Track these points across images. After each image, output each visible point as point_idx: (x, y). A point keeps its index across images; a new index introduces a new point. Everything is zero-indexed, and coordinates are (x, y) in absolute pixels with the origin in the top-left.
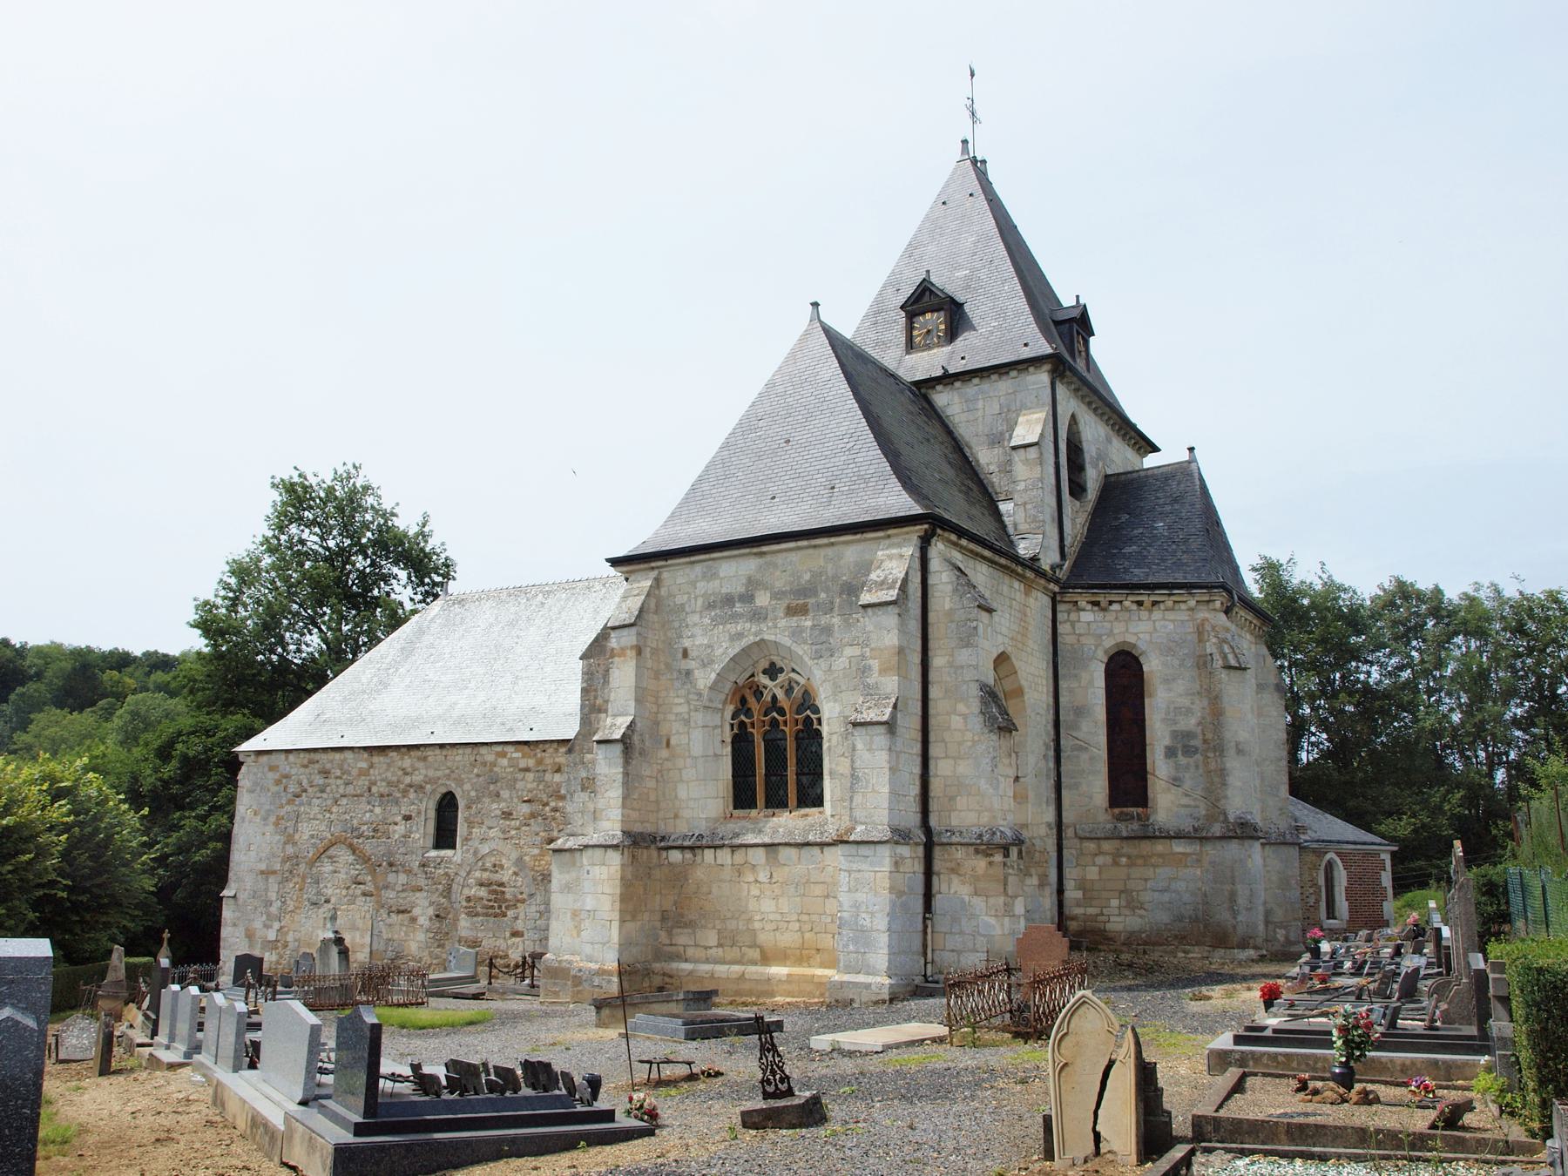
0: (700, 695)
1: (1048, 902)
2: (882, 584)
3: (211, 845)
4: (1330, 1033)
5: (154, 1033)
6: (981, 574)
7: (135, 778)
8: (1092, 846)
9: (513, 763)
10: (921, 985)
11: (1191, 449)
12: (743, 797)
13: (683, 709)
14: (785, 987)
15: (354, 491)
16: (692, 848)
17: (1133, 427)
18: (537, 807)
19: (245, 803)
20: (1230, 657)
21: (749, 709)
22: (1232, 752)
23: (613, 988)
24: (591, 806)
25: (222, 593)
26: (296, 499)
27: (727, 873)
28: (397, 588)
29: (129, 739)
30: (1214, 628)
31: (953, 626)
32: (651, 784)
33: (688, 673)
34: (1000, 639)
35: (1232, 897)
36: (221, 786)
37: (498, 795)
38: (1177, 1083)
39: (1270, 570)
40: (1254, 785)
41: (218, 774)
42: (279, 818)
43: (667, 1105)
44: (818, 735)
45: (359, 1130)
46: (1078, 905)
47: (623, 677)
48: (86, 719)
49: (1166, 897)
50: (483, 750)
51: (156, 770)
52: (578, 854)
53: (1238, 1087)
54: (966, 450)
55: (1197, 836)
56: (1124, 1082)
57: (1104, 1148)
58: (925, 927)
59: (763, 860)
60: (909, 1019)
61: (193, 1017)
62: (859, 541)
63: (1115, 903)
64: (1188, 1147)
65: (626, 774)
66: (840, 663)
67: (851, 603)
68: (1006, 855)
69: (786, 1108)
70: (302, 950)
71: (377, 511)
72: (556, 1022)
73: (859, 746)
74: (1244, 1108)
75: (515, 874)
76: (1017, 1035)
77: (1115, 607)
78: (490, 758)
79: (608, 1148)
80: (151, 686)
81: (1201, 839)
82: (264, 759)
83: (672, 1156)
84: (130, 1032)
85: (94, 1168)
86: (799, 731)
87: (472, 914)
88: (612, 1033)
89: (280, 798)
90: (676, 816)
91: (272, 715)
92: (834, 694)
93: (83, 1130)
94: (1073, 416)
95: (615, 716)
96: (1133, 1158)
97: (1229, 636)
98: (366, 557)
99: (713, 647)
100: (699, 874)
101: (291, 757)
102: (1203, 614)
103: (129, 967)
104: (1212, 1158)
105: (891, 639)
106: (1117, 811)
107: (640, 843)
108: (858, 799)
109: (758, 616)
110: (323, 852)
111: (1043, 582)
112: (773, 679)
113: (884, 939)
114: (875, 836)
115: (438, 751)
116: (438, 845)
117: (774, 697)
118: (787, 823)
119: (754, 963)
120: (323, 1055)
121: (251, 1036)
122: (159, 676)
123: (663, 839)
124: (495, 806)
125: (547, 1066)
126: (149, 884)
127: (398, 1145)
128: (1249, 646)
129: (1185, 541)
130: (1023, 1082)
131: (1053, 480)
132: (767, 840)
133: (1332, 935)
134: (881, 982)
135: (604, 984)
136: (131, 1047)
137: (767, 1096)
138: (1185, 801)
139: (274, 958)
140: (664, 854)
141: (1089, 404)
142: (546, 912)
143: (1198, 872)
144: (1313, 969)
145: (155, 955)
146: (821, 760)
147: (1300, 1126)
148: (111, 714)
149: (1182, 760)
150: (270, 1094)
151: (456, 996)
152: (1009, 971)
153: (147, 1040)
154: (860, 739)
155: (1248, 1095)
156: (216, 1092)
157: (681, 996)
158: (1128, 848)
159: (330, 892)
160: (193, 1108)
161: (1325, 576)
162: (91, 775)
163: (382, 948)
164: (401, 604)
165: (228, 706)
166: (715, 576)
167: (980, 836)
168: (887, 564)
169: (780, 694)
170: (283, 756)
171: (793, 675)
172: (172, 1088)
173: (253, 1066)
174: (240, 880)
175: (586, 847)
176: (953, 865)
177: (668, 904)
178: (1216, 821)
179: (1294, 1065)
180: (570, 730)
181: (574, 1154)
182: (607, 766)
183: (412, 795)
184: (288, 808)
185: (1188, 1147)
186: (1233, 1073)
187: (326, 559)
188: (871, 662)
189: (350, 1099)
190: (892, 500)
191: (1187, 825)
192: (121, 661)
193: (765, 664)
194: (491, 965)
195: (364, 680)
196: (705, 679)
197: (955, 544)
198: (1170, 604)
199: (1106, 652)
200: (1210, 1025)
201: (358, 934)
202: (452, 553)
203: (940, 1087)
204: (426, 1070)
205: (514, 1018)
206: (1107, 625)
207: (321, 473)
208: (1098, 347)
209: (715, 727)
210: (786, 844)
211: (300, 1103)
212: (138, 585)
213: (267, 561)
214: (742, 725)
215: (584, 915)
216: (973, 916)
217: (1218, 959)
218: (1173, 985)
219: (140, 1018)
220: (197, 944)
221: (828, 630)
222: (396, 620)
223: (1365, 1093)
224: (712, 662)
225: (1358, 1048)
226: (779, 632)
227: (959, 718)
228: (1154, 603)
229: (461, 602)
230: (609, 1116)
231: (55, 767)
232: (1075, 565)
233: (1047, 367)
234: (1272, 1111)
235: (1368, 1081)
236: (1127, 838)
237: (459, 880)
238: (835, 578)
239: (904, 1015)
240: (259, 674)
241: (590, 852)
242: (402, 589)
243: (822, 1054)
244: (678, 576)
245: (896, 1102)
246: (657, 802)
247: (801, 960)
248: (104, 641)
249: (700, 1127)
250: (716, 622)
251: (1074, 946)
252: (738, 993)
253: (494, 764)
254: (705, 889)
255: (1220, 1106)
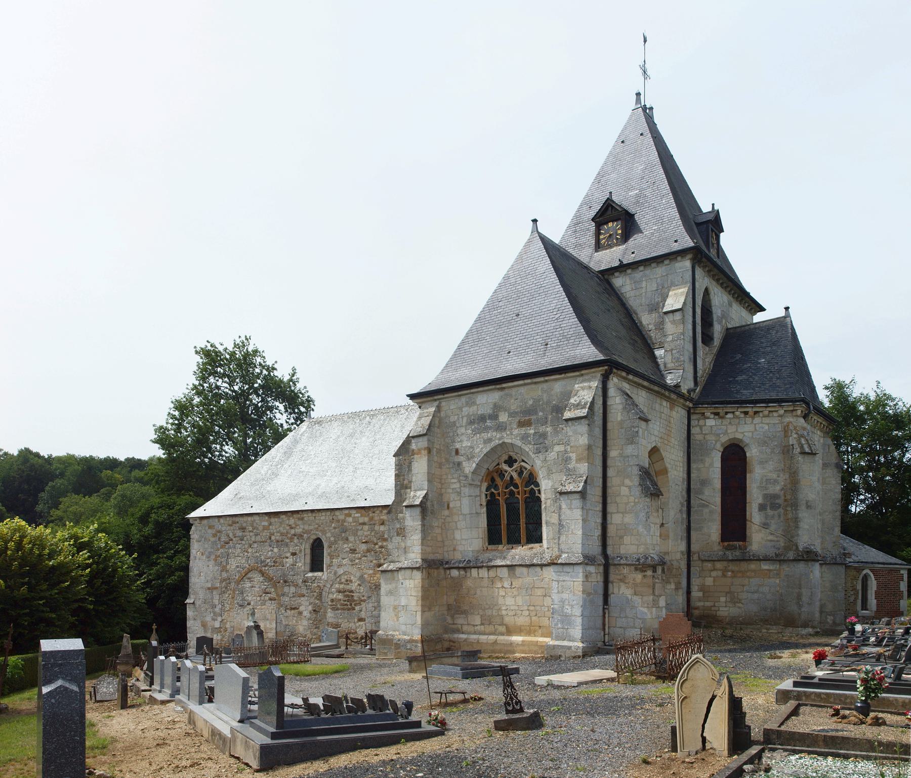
0: (466, 477)
1: (681, 599)
2: (578, 406)
3: (177, 574)
4: (855, 682)
5: (152, 684)
6: (641, 397)
7: (127, 535)
8: (709, 565)
9: (355, 520)
10: (599, 647)
11: (787, 309)
12: (493, 538)
13: (457, 486)
14: (521, 648)
15: (247, 355)
16: (464, 568)
17: (747, 295)
18: (371, 546)
19: (195, 549)
20: (806, 447)
21: (496, 485)
22: (803, 507)
23: (418, 650)
24: (403, 545)
25: (171, 421)
26: (211, 360)
27: (486, 582)
28: (278, 415)
29: (122, 511)
30: (795, 428)
31: (623, 431)
32: (438, 531)
33: (459, 464)
34: (653, 438)
35: (799, 597)
36: (180, 538)
37: (347, 539)
38: (756, 709)
39: (839, 390)
40: (816, 528)
41: (177, 531)
42: (217, 557)
43: (451, 718)
44: (539, 500)
45: (274, 736)
46: (700, 601)
47: (420, 467)
48: (93, 500)
49: (756, 596)
50: (337, 513)
51: (140, 530)
52: (396, 573)
53: (795, 712)
54: (634, 315)
55: (778, 559)
56: (721, 709)
57: (708, 746)
58: (604, 613)
59: (506, 575)
60: (594, 667)
61: (173, 675)
62: (563, 378)
63: (723, 599)
64: (759, 747)
65: (423, 525)
66: (552, 455)
67: (558, 418)
68: (655, 571)
69: (519, 719)
70: (236, 633)
71: (263, 367)
72: (386, 670)
73: (564, 506)
74: (796, 725)
75: (359, 585)
76: (658, 678)
77: (730, 416)
78: (341, 517)
79: (418, 743)
80: (132, 479)
81: (780, 561)
82: (205, 522)
83: (455, 746)
84: (138, 684)
85: (122, 761)
86: (527, 498)
87: (334, 609)
88: (418, 676)
89: (217, 545)
90: (454, 550)
91: (209, 495)
92: (548, 475)
93: (114, 740)
94: (706, 290)
95: (416, 490)
96: (726, 752)
97: (805, 433)
98: (258, 395)
99: (474, 447)
100: (469, 583)
101: (222, 520)
102: (788, 419)
103: (133, 645)
104: (775, 754)
105: (583, 440)
106: (726, 544)
107: (434, 567)
108: (563, 538)
109: (501, 428)
110: (245, 575)
111: (682, 401)
112: (511, 466)
113: (579, 621)
114: (573, 560)
115: (310, 514)
116: (313, 570)
117: (512, 477)
118: (521, 553)
119: (502, 634)
120: (251, 693)
121: (208, 684)
122: (137, 473)
123: (447, 563)
124: (346, 546)
125: (381, 697)
126: (141, 598)
127: (297, 744)
128: (819, 439)
129: (779, 371)
130: (661, 705)
131: (691, 333)
132: (509, 563)
133: (863, 620)
134: (578, 645)
135: (413, 648)
136: (138, 692)
137: (508, 712)
138: (771, 537)
139: (219, 638)
140: (448, 572)
141: (717, 281)
142: (378, 607)
143: (778, 581)
144: (849, 641)
145: (148, 638)
146: (541, 514)
147: (832, 737)
148: (110, 497)
149: (770, 512)
150: (221, 717)
151: (327, 656)
152: (654, 640)
153: (148, 688)
154: (564, 503)
155: (801, 718)
156: (190, 717)
157: (460, 654)
158: (732, 567)
159: (250, 599)
160: (177, 726)
161: (878, 391)
162: (100, 535)
163: (283, 629)
164: (282, 425)
165: (180, 491)
166: (474, 403)
167: (638, 560)
168: (581, 393)
169: (515, 475)
170: (216, 520)
171: (523, 464)
172: (164, 715)
173: (210, 701)
174: (196, 593)
175: (401, 569)
176: (622, 577)
177: (451, 601)
178: (791, 550)
179: (832, 700)
180: (389, 499)
181: (399, 746)
182: (412, 521)
183: (296, 541)
184: (222, 550)
185: (759, 747)
186: (792, 704)
187: (233, 398)
188: (571, 454)
189: (268, 718)
190: (584, 351)
191: (771, 552)
192: (111, 464)
193: (505, 457)
194: (347, 638)
195: (263, 473)
196: (469, 467)
197: (625, 379)
198: (766, 413)
199: (722, 445)
200: (780, 673)
201: (268, 622)
202: (312, 394)
203: (611, 707)
204: (312, 701)
205: (361, 668)
206: (724, 427)
207: (225, 342)
208: (725, 240)
209: (476, 496)
210: (520, 565)
211: (239, 722)
212: (118, 417)
213: (197, 400)
214: (492, 494)
215: (400, 608)
216: (633, 607)
217: (788, 634)
218: (758, 649)
219: (143, 675)
220: (174, 633)
221: (544, 436)
222: (279, 436)
223: (877, 719)
224: (473, 457)
225: (873, 692)
226: (513, 436)
227: (626, 489)
228: (756, 413)
229: (319, 422)
230: (418, 724)
231: (77, 530)
232: (704, 388)
233: (690, 256)
234: (815, 728)
235: (879, 712)
236: (732, 560)
237: (326, 589)
238: (548, 402)
239: (591, 665)
240: (198, 470)
241: (403, 572)
242: (281, 417)
243: (541, 687)
244: (451, 405)
245: (584, 716)
246: (443, 541)
247: (529, 633)
248: (101, 453)
249: (469, 735)
250: (476, 432)
251: (696, 625)
252: (494, 651)
253: (344, 521)
254: (472, 592)
255: (782, 724)
